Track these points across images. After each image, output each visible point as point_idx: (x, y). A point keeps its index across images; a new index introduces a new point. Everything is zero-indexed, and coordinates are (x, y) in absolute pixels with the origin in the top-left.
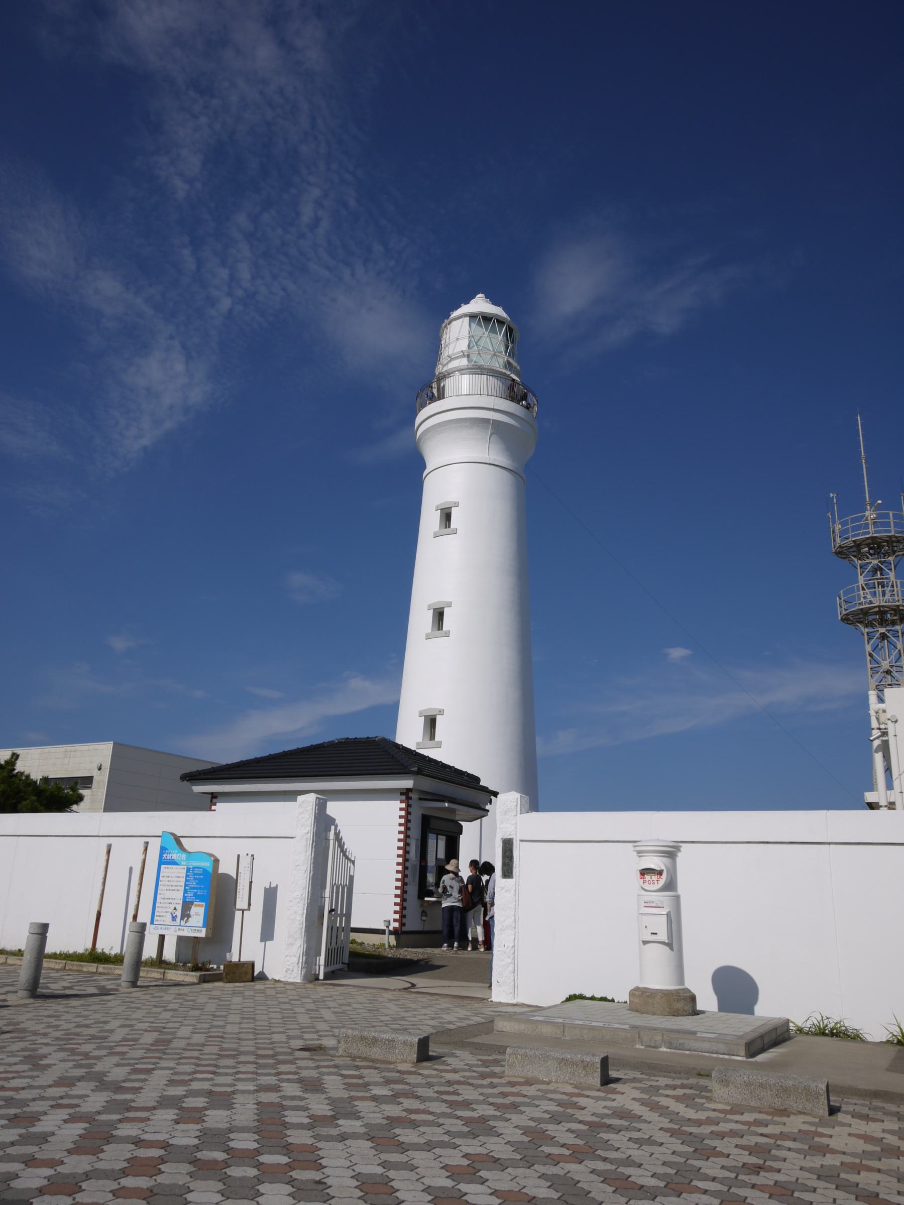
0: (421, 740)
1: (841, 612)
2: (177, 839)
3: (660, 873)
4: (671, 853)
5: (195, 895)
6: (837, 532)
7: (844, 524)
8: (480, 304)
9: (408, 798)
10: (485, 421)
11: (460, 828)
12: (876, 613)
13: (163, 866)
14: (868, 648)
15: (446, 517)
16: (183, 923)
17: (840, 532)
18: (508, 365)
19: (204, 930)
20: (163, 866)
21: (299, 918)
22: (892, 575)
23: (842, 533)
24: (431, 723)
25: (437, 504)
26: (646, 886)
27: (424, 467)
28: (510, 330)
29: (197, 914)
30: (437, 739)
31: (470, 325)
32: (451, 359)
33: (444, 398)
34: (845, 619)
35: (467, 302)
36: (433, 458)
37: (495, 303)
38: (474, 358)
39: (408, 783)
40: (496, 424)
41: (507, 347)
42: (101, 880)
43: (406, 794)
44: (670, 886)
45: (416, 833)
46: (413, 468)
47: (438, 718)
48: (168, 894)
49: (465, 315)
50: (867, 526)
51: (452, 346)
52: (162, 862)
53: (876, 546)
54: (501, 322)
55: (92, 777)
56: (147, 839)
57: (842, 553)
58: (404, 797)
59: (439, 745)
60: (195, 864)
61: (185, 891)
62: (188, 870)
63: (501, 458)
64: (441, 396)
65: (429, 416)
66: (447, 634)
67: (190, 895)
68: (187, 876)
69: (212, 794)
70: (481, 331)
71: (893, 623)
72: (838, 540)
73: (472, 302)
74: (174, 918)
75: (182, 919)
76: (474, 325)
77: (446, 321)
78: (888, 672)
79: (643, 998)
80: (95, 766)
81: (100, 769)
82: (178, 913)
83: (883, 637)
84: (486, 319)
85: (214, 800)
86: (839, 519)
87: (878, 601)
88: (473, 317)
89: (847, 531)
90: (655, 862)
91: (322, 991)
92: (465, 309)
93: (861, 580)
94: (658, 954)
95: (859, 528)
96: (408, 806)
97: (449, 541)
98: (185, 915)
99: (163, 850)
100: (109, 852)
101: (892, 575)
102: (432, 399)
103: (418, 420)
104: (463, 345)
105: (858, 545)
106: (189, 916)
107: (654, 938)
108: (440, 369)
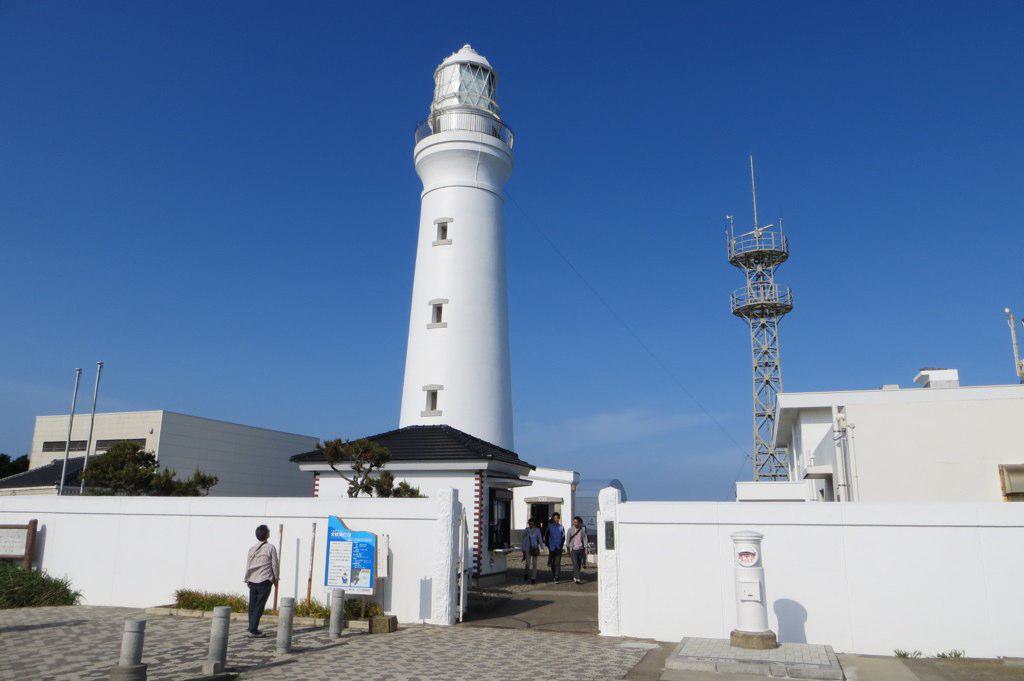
0: (424, 410)
1: (733, 308)
2: (340, 520)
3: (754, 555)
4: (757, 541)
5: (362, 563)
6: (733, 246)
7: (738, 240)
8: (466, 54)
9: (482, 476)
10: (475, 152)
11: (511, 493)
12: (759, 309)
13: (331, 543)
14: (753, 335)
15: (443, 229)
16: (353, 584)
17: (735, 246)
18: (491, 106)
19: (371, 590)
20: (331, 543)
21: (444, 579)
22: (771, 280)
23: (737, 247)
24: (433, 396)
25: (435, 218)
26: (743, 563)
27: (421, 188)
28: (492, 77)
29: (365, 578)
30: (438, 408)
31: (461, 72)
32: (445, 98)
33: (439, 131)
34: (737, 313)
35: (456, 52)
36: (429, 183)
37: (480, 53)
38: (464, 99)
39: (483, 465)
40: (484, 155)
41: (490, 90)
42: (310, 562)
43: (479, 472)
44: (758, 564)
45: (486, 502)
46: (412, 189)
47: (439, 392)
48: (338, 563)
49: (457, 63)
50: (754, 243)
51: (445, 88)
52: (330, 539)
53: (760, 257)
54: (485, 70)
55: (145, 440)
56: (314, 520)
57: (735, 262)
58: (478, 476)
59: (440, 413)
60: (359, 540)
61: (353, 561)
62: (354, 545)
63: (487, 185)
64: (437, 130)
65: (425, 148)
66: (445, 325)
67: (357, 564)
68: (353, 550)
69: (315, 472)
70: (470, 77)
71: (771, 315)
72: (733, 252)
73: (461, 51)
74: (345, 581)
75: (352, 581)
76: (464, 71)
77: (440, 66)
78: (766, 353)
79: (740, 639)
80: (148, 430)
81: (152, 433)
82: (348, 577)
83: (763, 326)
84: (474, 67)
85: (317, 477)
86: (735, 235)
87: (762, 300)
88: (463, 64)
89: (740, 246)
90: (751, 548)
91: (459, 628)
92: (455, 57)
93: (749, 283)
94: (751, 609)
95: (749, 243)
96: (482, 482)
97: (444, 251)
98: (354, 578)
99: (330, 530)
100: (281, 531)
101: (771, 280)
102: (428, 133)
103: (416, 151)
104: (455, 87)
105: (748, 256)
106: (357, 580)
107: (750, 598)
108: (435, 107)
